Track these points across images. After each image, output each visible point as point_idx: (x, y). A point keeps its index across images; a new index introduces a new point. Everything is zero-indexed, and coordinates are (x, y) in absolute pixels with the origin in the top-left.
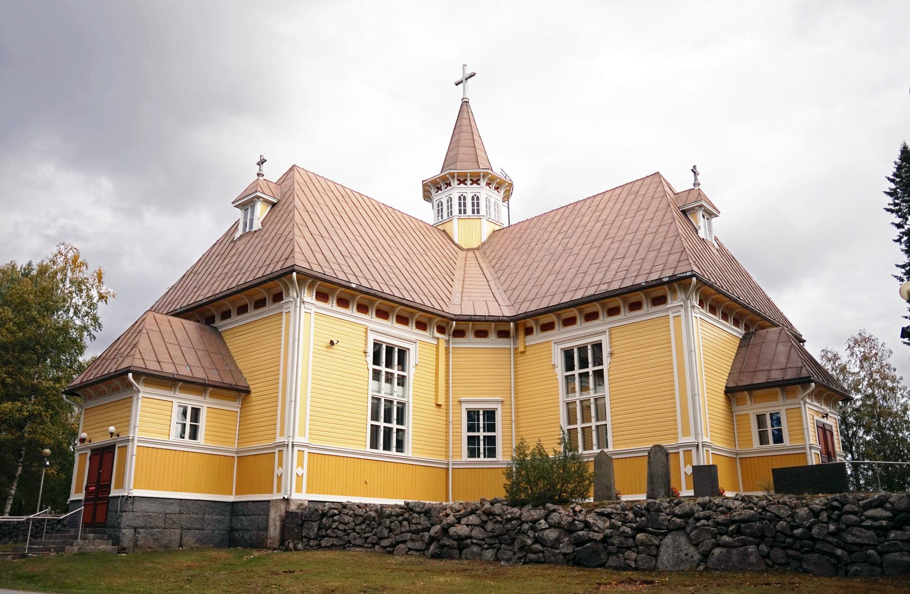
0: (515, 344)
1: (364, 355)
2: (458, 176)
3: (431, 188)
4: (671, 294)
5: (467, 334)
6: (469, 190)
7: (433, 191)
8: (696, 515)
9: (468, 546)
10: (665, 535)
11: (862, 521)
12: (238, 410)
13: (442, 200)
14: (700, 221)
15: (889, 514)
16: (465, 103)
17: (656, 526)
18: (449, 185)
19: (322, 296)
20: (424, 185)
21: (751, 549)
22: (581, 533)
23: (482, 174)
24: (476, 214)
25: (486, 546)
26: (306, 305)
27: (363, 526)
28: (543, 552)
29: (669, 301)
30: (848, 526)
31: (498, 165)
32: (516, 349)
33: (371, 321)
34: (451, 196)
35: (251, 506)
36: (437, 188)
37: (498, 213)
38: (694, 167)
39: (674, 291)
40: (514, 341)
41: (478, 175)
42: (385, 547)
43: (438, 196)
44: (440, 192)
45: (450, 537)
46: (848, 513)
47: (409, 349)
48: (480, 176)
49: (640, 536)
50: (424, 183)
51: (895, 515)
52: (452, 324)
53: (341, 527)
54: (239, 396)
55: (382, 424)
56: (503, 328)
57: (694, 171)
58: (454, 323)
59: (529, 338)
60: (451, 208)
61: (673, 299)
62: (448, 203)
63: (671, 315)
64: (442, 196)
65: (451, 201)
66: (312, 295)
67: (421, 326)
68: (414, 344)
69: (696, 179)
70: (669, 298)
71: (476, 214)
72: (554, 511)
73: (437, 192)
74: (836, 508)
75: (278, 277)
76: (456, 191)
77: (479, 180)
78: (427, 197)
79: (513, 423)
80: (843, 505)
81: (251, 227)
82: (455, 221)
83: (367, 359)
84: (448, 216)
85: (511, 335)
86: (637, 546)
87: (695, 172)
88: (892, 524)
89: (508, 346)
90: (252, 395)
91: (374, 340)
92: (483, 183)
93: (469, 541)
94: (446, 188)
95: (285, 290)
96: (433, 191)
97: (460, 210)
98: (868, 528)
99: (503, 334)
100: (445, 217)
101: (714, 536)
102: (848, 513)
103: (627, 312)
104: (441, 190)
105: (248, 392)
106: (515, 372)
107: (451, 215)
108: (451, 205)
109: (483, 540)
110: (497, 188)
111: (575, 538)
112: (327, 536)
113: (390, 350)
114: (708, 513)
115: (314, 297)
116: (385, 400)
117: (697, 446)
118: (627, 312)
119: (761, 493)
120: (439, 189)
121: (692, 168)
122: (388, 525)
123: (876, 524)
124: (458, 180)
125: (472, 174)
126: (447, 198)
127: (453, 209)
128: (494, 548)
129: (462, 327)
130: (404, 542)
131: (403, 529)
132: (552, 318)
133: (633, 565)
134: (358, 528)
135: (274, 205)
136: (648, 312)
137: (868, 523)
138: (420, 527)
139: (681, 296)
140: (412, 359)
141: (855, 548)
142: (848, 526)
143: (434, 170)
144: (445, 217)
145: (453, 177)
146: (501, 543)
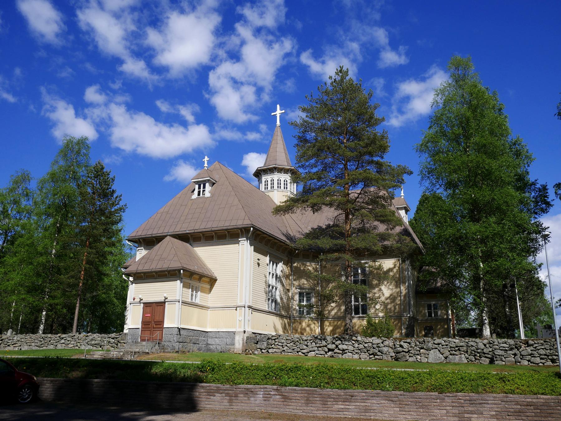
8: (442, 344)
9: (346, 353)
10: (430, 350)
11: (500, 348)
15: (508, 346)
17: (427, 347)
21: (463, 356)
22: (398, 349)
24: (286, 189)
25: (355, 353)
27: (291, 344)
28: (382, 355)
30: (495, 349)
45: (339, 349)
46: (495, 345)
49: (422, 350)
51: (510, 346)
53: (280, 344)
60: (273, 184)
71: (286, 189)
72: (385, 340)
74: (492, 343)
80: (494, 342)
86: (421, 354)
88: (509, 349)
93: (347, 351)
97: (284, 187)
98: (501, 350)
100: (269, 188)
101: (449, 351)
102: (495, 345)
107: (273, 188)
109: (354, 351)
111: (396, 351)
112: (272, 348)
114: (447, 343)
116: (167, 276)
117: (245, 307)
119: (199, 363)
122: (306, 344)
123: (504, 349)
127: (271, 182)
128: (359, 354)
130: (314, 351)
131: (313, 346)
133: (419, 361)
134: (288, 345)
137: (501, 348)
138: (321, 345)
141: (497, 356)
142: (495, 349)
144: (269, 188)
146: (361, 352)
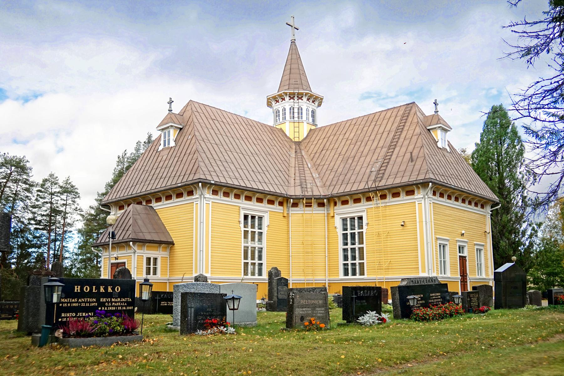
0: (327, 211)
1: (239, 223)
2: (289, 94)
3: (272, 100)
4: (417, 189)
5: (299, 206)
6: (296, 104)
7: (273, 103)
12: (168, 256)
13: (279, 109)
14: (438, 135)
16: (293, 42)
18: (283, 99)
19: (215, 192)
20: (268, 99)
23: (304, 94)
26: (207, 199)
29: (416, 194)
31: (315, 90)
32: (328, 214)
33: (242, 203)
34: (285, 107)
35: (133, 293)
36: (276, 101)
37: (314, 118)
38: (436, 100)
39: (418, 188)
40: (327, 209)
41: (302, 94)
42: (44, 236)
43: (276, 106)
44: (278, 103)
47: (264, 216)
48: (303, 95)
50: (268, 97)
52: (290, 201)
54: (168, 247)
55: (249, 261)
56: (321, 201)
57: (435, 104)
58: (292, 200)
59: (335, 208)
60: (285, 115)
61: (419, 193)
62: (283, 111)
63: (417, 203)
64: (279, 106)
65: (285, 111)
66: (210, 193)
67: (271, 202)
68: (267, 213)
69: (436, 109)
70: (416, 192)
73: (276, 104)
75: (192, 184)
76: (287, 104)
77: (302, 97)
78: (269, 105)
79: (327, 257)
81: (169, 144)
82: (287, 123)
83: (241, 225)
84: (283, 120)
85: (326, 205)
87: (435, 104)
89: (323, 212)
90: (175, 245)
91: (244, 213)
92: (305, 99)
94: (282, 101)
95: (195, 190)
96: (273, 103)
99: (321, 205)
103: (390, 198)
104: (279, 102)
105: (172, 243)
106: (328, 228)
107: (285, 119)
108: (285, 113)
110: (313, 102)
113: (253, 217)
115: (211, 194)
118: (390, 198)
120: (277, 101)
121: (434, 102)
124: (289, 97)
125: (298, 94)
126: (283, 108)
129: (296, 201)
132: (348, 198)
135: (181, 129)
136: (403, 198)
139: (421, 191)
140: (266, 222)
143: (274, 92)
145: (286, 95)
